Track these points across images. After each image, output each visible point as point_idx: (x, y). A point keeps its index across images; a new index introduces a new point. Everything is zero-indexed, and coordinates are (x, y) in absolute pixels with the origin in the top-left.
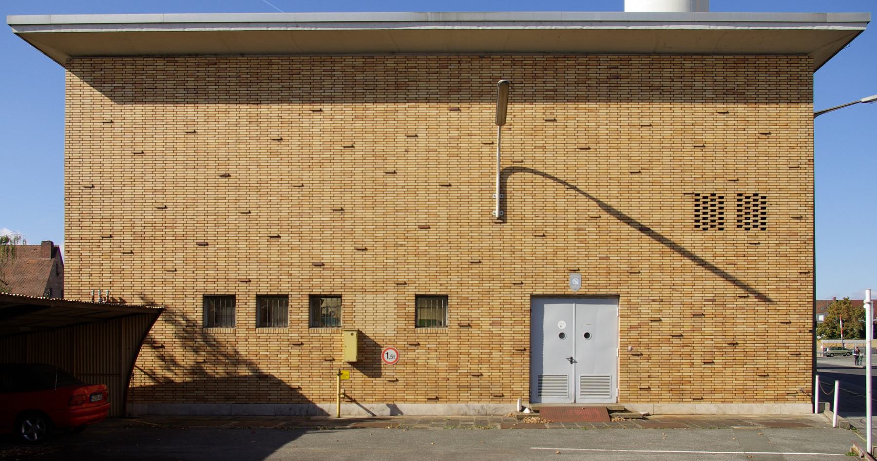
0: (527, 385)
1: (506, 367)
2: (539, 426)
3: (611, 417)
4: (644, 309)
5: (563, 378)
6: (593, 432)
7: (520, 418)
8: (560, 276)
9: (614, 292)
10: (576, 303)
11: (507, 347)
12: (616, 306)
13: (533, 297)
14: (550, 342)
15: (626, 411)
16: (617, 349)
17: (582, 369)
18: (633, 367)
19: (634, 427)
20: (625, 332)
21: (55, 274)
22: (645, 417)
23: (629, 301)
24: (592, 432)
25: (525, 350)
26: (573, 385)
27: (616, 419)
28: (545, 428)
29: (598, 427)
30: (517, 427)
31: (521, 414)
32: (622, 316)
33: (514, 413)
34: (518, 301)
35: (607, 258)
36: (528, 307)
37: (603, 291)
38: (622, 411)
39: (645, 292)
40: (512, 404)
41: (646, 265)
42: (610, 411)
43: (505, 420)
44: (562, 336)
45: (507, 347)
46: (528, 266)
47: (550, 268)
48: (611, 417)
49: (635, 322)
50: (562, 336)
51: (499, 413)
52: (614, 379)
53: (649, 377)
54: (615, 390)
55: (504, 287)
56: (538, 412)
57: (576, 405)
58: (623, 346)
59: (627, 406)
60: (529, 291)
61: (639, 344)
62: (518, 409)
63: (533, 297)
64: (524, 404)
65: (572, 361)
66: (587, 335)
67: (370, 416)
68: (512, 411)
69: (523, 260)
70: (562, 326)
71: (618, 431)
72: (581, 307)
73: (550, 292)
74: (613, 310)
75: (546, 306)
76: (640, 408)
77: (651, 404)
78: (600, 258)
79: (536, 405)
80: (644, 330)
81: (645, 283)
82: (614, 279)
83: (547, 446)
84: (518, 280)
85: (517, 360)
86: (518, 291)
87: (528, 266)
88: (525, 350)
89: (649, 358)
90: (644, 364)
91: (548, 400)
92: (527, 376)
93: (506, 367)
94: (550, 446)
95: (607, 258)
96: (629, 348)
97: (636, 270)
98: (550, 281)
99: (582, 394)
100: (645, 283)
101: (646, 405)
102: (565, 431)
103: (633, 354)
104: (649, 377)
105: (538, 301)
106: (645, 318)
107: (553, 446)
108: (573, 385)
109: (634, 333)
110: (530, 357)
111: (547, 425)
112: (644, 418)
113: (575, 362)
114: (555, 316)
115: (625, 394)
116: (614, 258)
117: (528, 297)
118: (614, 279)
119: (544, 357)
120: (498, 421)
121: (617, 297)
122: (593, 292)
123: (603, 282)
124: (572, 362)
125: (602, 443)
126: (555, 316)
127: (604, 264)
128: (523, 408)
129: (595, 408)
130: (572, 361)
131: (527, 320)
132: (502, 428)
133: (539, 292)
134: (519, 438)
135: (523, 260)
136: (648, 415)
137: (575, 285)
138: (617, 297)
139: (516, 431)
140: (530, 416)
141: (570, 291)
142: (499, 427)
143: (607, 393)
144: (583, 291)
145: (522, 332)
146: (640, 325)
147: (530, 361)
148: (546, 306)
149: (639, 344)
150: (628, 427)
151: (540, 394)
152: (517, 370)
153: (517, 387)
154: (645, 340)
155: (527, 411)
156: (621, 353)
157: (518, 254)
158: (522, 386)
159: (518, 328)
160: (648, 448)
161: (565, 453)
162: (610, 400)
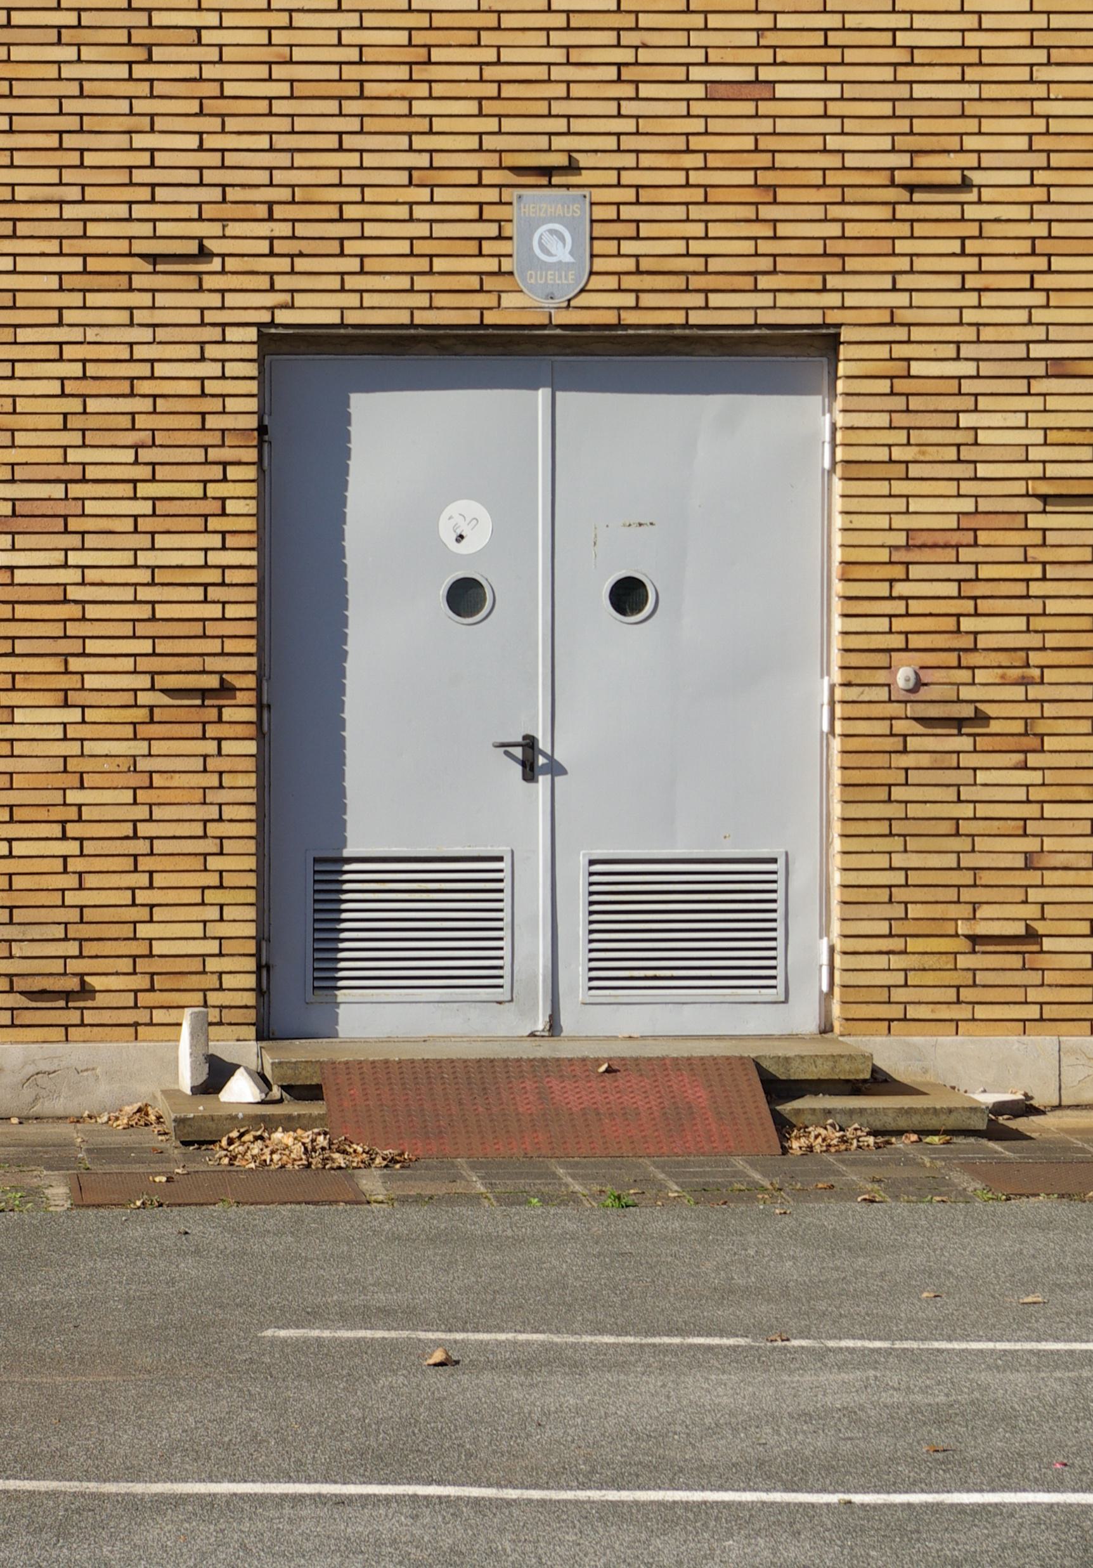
0: (241, 924)
1: (106, 800)
2: (319, 1184)
3: (784, 1127)
4: (1000, 425)
5: (471, 885)
6: (665, 1221)
7: (197, 1138)
8: (453, 209)
9: (800, 310)
10: (556, 387)
11: (107, 675)
12: (815, 402)
13: (275, 342)
14: (387, 635)
15: (879, 1082)
16: (822, 686)
17: (611, 815)
18: (927, 798)
19: (932, 1187)
20: (876, 577)
21: (974, 1105)
22: (1003, 1123)
23: (899, 375)
24: (658, 1222)
25: (226, 690)
26: (544, 922)
27: (819, 1136)
28: (360, 1200)
29: (705, 1193)
30: (173, 1197)
31: (202, 1107)
32: (853, 470)
33: (161, 1106)
34: (179, 373)
35: (760, 90)
36: (243, 411)
37: (732, 309)
38: (855, 1088)
39: (1005, 311)
40: (147, 1047)
41: (1007, 134)
42: (778, 1088)
43: (98, 1152)
44: (465, 597)
45: (107, 675)
46: (243, 141)
47: (389, 155)
48: (784, 1127)
49: (936, 508)
50: (465, 597)
51: (58, 1106)
52: (804, 878)
53: (1030, 862)
54: (812, 944)
55: (86, 278)
56: (311, 1093)
57: (563, 1049)
58: (862, 664)
59: (889, 1052)
60: (253, 306)
61: (965, 653)
62: (186, 1081)
63: (275, 342)
64: (225, 1046)
65: (530, 760)
66: (628, 596)
67: (549, 753)
68: (146, 1089)
69: (212, 104)
70: (468, 532)
71: (828, 1215)
72: (582, 407)
73: (386, 311)
74: (798, 427)
75: (362, 405)
76: (976, 1065)
77: (1044, 1042)
78: (713, 91)
79: (299, 1051)
80: (999, 557)
81: (1006, 254)
82: (803, 226)
83: (366, 1316)
84: (178, 236)
85: (177, 754)
86: (179, 305)
87: (243, 141)
88: (226, 690)
89: (1030, 739)
90: (1000, 781)
91: (374, 1018)
92: (240, 862)
93: (106, 800)
94: (385, 1315)
95: (760, 90)
96: (903, 676)
97: (942, 167)
98: (386, 243)
99: (600, 976)
100: (1006, 254)
101: (1012, 1043)
102: (487, 1219)
103: (925, 714)
104: (1030, 862)
105: (311, 369)
106: (1003, 483)
107: (411, 1317)
108: (544, 922)
109: (932, 582)
110: (261, 735)
111: (372, 1183)
112: (995, 1133)
113: (556, 769)
114: (416, 469)
115: (879, 973)
116: (800, 87)
117: (243, 344)
118: (803, 226)
119: (350, 734)
120: (55, 1157)
121: (825, 342)
122: (663, 310)
123: (730, 247)
124: (530, 771)
125: (726, 1293)
126: (416, 469)
127: (735, 126)
128: (217, 1074)
129: (690, 1063)
130: (530, 760)
131: (240, 495)
132: (81, 1199)
133: (315, 311)
134: (188, 1266)
135: (212, 104)
136: (1025, 1108)
137: (550, 261)
138: (825, 342)
139: (167, 1225)
140: (261, 1123)
141: (516, 308)
142: (58, 1193)
143: (754, 964)
144: (602, 307)
145: (205, 574)
146: (969, 528)
147: (263, 765)
148: (362, 405)
149: (965, 653)
150: (895, 1190)
151: (325, 979)
152: (177, 817)
153: (175, 935)
154: (1001, 628)
155: (241, 1090)
156: (849, 709)
157: (174, 62)
158: (209, 925)
159: (179, 551)
160: (1023, 1322)
161: (489, 1360)
162: (783, 1017)
